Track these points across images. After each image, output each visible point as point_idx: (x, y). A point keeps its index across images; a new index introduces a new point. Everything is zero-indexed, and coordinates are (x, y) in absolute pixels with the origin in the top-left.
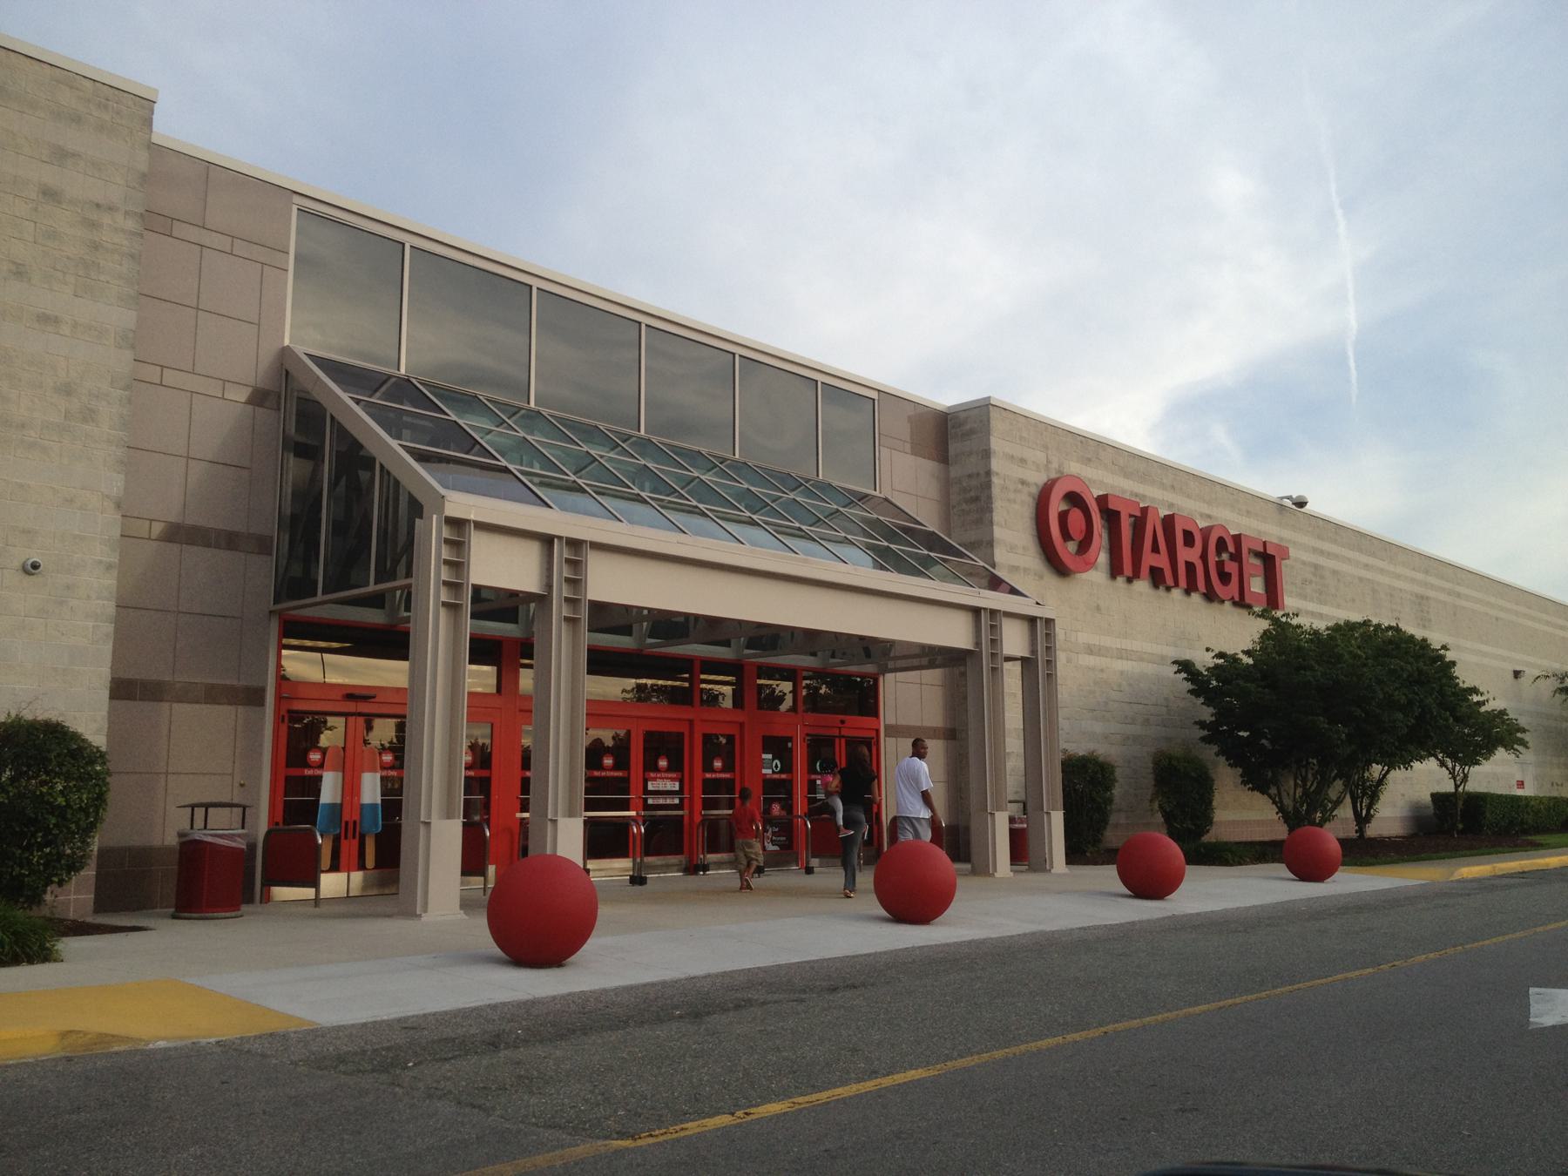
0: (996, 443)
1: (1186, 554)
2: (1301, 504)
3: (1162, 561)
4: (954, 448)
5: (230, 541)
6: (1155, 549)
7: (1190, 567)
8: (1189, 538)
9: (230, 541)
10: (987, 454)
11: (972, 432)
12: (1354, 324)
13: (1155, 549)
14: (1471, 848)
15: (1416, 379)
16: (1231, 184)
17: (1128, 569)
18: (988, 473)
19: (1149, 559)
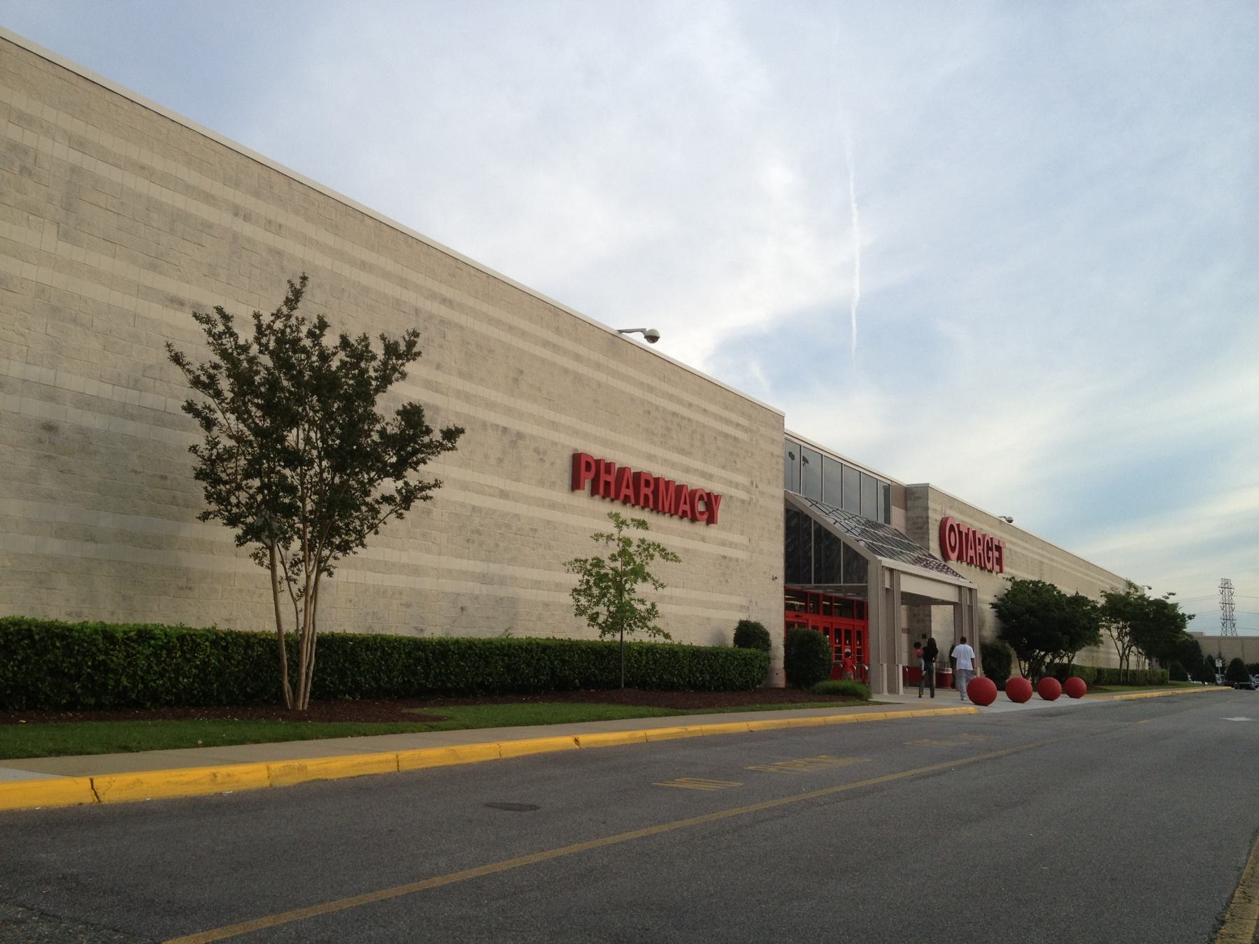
0: (931, 505)
1: (645, 491)
2: (1010, 521)
3: (971, 553)
4: (909, 503)
5: (1227, 604)
6: (628, 487)
7: (646, 496)
8: (647, 483)
9: (1227, 604)
10: (927, 509)
11: (919, 498)
12: (857, 293)
13: (628, 487)
14: (793, 702)
15: (894, 339)
16: (778, 177)
17: (612, 495)
18: (927, 517)
19: (624, 491)
